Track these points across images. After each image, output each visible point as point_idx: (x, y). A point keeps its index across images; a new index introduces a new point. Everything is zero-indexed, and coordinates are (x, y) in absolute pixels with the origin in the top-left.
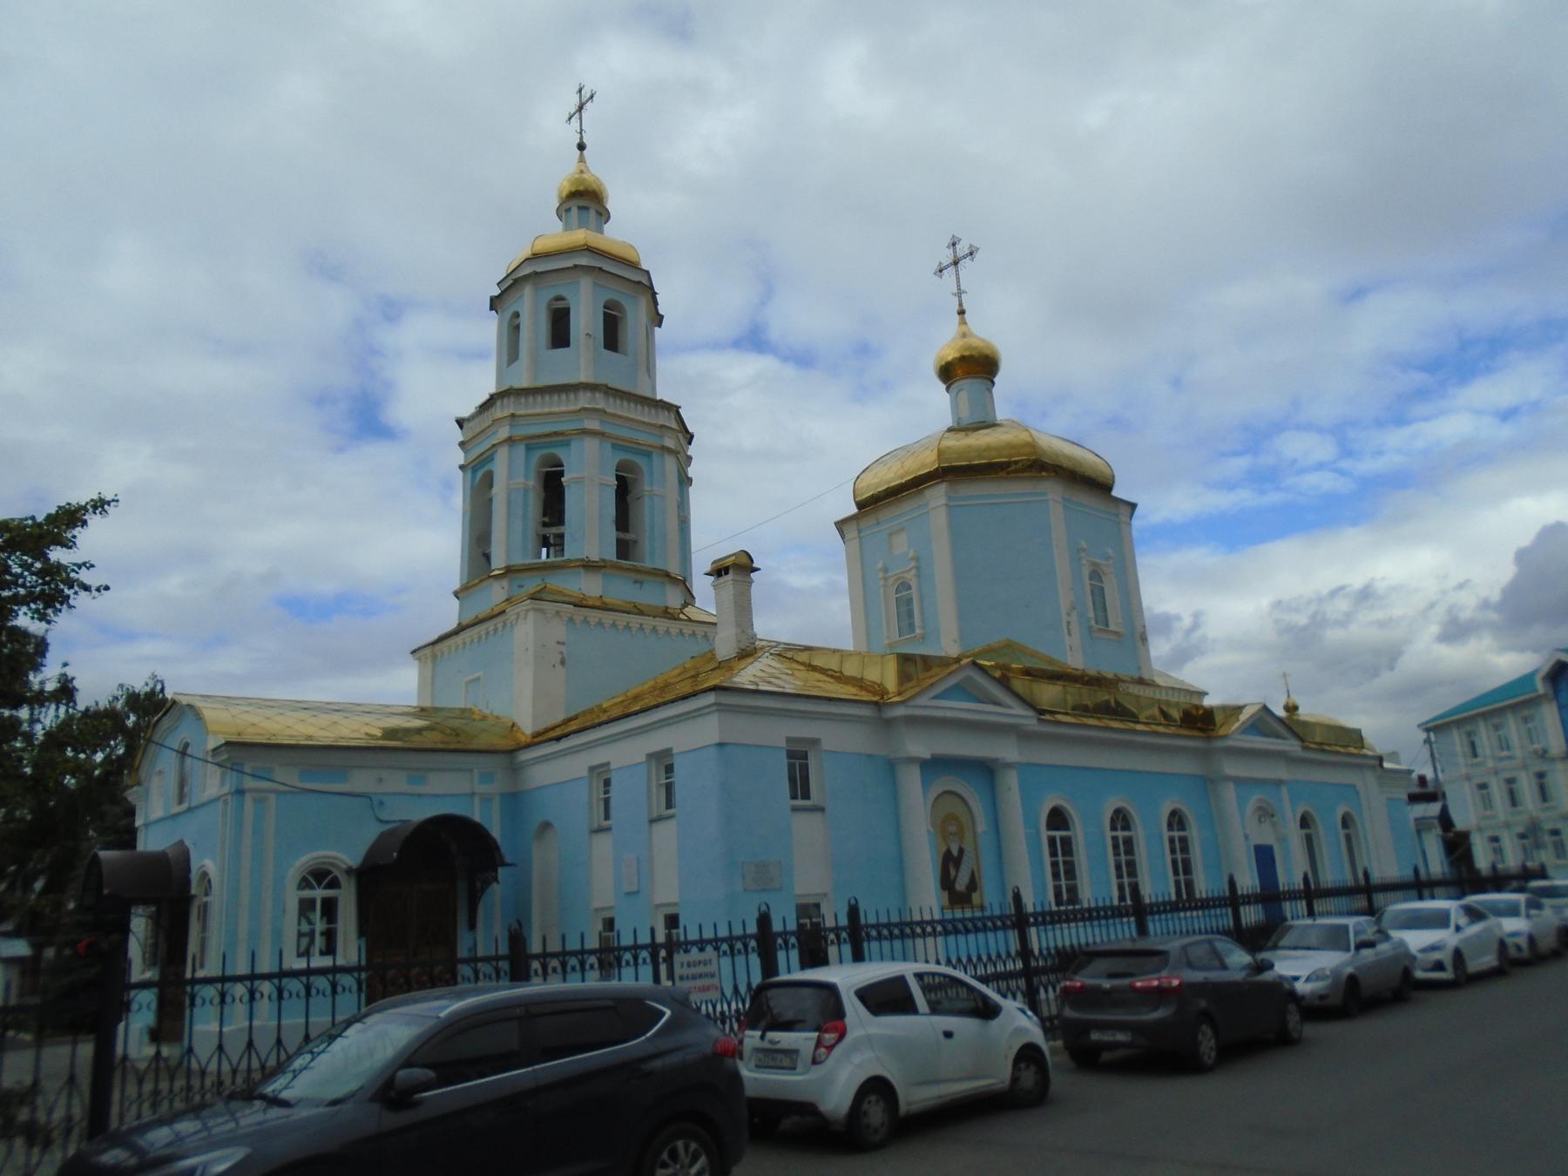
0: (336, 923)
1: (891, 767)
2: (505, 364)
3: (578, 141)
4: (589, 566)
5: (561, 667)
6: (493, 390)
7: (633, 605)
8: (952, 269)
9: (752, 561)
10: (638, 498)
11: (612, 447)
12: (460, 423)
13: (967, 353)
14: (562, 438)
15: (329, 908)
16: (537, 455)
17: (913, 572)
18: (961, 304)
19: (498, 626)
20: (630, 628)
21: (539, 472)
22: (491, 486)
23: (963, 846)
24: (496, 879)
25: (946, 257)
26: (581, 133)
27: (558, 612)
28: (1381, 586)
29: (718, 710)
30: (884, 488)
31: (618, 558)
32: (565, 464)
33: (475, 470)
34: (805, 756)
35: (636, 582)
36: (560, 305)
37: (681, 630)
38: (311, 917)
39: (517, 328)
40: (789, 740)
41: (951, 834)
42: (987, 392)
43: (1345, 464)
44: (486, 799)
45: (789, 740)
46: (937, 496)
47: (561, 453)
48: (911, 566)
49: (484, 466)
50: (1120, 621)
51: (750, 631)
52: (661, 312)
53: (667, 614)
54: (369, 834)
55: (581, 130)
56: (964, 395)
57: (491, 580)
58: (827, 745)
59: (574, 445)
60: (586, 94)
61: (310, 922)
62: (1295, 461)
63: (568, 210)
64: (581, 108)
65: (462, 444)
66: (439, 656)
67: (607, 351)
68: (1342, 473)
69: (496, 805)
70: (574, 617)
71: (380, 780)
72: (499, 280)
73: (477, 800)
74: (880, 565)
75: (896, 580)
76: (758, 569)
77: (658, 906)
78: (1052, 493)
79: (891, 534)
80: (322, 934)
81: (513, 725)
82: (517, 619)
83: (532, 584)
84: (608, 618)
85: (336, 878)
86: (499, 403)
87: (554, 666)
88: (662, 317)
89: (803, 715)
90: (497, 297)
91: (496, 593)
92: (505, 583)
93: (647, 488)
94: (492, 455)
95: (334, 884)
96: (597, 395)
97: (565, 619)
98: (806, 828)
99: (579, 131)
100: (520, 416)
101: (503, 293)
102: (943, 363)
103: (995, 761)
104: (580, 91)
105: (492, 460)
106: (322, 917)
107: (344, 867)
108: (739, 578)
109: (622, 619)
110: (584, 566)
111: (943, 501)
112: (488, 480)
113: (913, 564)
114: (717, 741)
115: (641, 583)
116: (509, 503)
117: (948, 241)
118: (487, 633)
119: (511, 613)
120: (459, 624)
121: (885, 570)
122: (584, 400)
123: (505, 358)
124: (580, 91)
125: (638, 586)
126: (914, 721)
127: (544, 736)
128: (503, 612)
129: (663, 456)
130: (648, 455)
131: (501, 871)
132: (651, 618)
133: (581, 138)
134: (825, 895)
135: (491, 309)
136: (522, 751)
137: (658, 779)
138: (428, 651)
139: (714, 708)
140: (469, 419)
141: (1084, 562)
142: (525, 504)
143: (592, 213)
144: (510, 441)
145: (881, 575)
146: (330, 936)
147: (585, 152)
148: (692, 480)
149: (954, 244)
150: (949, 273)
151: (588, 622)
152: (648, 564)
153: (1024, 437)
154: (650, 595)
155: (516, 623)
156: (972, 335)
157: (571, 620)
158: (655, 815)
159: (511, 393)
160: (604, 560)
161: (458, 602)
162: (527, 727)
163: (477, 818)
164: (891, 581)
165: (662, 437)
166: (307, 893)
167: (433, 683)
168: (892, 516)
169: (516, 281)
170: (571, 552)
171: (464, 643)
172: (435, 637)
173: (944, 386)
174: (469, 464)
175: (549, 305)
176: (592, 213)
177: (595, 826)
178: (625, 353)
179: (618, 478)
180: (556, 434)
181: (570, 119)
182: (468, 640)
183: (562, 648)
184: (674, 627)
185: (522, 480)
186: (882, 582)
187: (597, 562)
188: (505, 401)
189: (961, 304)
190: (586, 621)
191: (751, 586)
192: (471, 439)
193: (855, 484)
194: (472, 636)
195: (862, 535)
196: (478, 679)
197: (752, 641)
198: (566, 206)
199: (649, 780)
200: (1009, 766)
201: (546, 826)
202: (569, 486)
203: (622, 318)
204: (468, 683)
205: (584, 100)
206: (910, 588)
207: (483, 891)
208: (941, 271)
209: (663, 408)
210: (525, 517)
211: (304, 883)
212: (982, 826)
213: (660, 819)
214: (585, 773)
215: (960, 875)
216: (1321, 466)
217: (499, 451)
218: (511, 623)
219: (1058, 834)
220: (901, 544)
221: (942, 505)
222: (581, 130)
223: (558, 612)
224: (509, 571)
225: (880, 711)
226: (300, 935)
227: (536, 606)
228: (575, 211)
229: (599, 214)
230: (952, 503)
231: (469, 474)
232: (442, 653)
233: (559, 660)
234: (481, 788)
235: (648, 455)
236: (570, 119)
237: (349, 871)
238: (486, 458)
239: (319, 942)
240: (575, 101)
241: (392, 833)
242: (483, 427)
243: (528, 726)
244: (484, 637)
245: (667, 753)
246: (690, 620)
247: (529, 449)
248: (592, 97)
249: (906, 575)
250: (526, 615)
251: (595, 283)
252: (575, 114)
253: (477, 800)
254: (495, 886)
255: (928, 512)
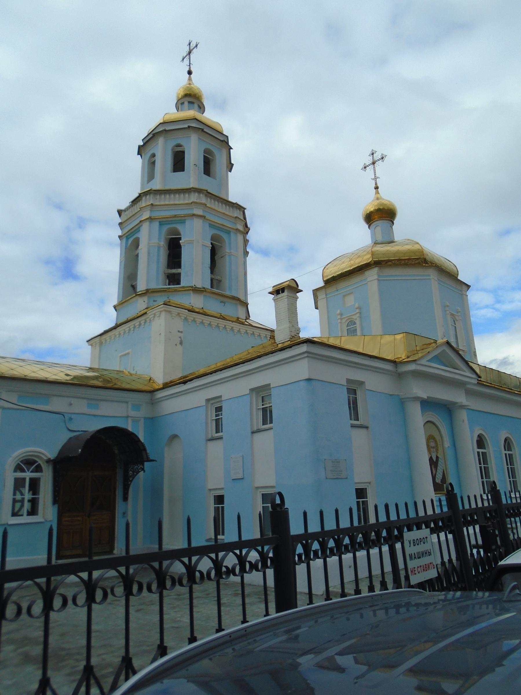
0: (39, 495)
1: (402, 402)
2: (146, 182)
3: (188, 69)
4: (196, 290)
5: (180, 345)
6: (140, 192)
7: (220, 314)
8: (372, 166)
9: (298, 286)
10: (222, 257)
11: (209, 226)
12: (120, 212)
13: (381, 207)
14: (182, 219)
15: (34, 485)
16: (166, 228)
17: (358, 315)
18: (376, 184)
19: (142, 322)
20: (219, 327)
21: (166, 238)
22: (137, 246)
23: (438, 455)
24: (143, 469)
25: (368, 160)
26: (190, 65)
27: (179, 314)
28: (511, 359)
29: (307, 357)
30: (340, 272)
31: (211, 288)
32: (182, 233)
33: (128, 238)
34: (354, 392)
35: (221, 302)
36: (179, 149)
37: (246, 331)
38: (23, 491)
39: (154, 163)
40: (349, 381)
41: (432, 447)
42: (390, 228)
43: (498, 306)
44: (136, 421)
45: (349, 381)
46: (372, 274)
47: (179, 227)
48: (357, 312)
49: (134, 235)
50: (465, 345)
51: (296, 326)
52: (232, 162)
53: (238, 321)
54: (64, 437)
55: (190, 64)
56: (379, 229)
57: (137, 297)
58: (368, 386)
59: (188, 222)
60: (193, 45)
61: (22, 494)
62: (476, 304)
63: (183, 103)
64: (190, 53)
65: (120, 224)
66: (104, 342)
67: (205, 175)
68: (497, 310)
69: (142, 423)
70: (188, 317)
71: (71, 404)
72: (143, 138)
73: (130, 420)
74: (338, 312)
75: (347, 320)
76: (301, 291)
77: (257, 488)
78: (432, 275)
79: (344, 296)
80: (29, 501)
81: (150, 379)
82: (154, 317)
83: (161, 299)
84: (207, 320)
85: (39, 465)
86: (144, 198)
87: (176, 345)
88: (232, 165)
89: (357, 366)
90: (142, 146)
91: (140, 304)
92: (145, 298)
93: (227, 251)
94: (139, 228)
95: (39, 469)
96: (201, 195)
97: (183, 318)
98: (358, 436)
99: (188, 65)
100: (156, 205)
101: (144, 144)
102: (368, 212)
103: (454, 403)
104: (190, 44)
105: (139, 231)
106: (29, 490)
107: (45, 458)
108: (290, 295)
109: (215, 321)
110: (192, 290)
111: (376, 277)
112: (136, 244)
113: (358, 311)
114: (307, 377)
115: (224, 303)
116: (149, 253)
117: (370, 152)
118: (134, 327)
119: (149, 314)
120: (116, 324)
121: (341, 314)
122: (194, 197)
123: (146, 179)
124: (190, 44)
125: (223, 304)
126: (418, 375)
127: (166, 386)
128: (146, 313)
129: (236, 234)
130: (228, 233)
131: (146, 464)
132: (231, 322)
133: (190, 68)
134: (370, 483)
135: (138, 154)
136: (159, 392)
137: (257, 405)
138: (97, 339)
139: (306, 355)
140: (125, 211)
141: (448, 312)
142: (158, 256)
143: (196, 106)
144: (151, 219)
145: (339, 317)
146: (34, 502)
147: (191, 75)
148: (249, 253)
149: (373, 154)
150: (370, 169)
151: (195, 321)
152: (228, 293)
153: (416, 247)
154: (229, 310)
155: (153, 319)
156: (381, 198)
157: (186, 319)
158: (255, 429)
159: (151, 193)
160: (204, 288)
161: (116, 312)
162: (160, 381)
163: (130, 429)
164: (344, 321)
165: (235, 224)
166: (221, 417)
167: (100, 358)
168: (344, 286)
169: (154, 135)
170: (184, 282)
171: (120, 334)
172: (101, 331)
173: (367, 226)
174: (125, 234)
175: (173, 149)
176: (196, 106)
177: (210, 437)
178: (215, 178)
179: (212, 244)
180: (175, 216)
181: (183, 60)
182: (122, 332)
183: (180, 334)
184: (243, 329)
185: (157, 241)
186: (339, 321)
187: (201, 288)
188: (148, 197)
189: (376, 184)
190: (194, 320)
191: (297, 300)
192: (124, 222)
193: (323, 271)
194: (124, 330)
195: (327, 297)
196: (128, 354)
197: (297, 332)
198: (180, 102)
199: (251, 404)
200: (462, 407)
201: (175, 437)
202: (184, 245)
203: (213, 160)
204: (121, 356)
205: (191, 48)
206: (355, 323)
207: (134, 477)
208: (365, 168)
209: (237, 208)
210: (158, 262)
211: (18, 468)
212: (447, 444)
213: (259, 431)
214: (248, 392)
215: (437, 473)
216: (487, 307)
217: (143, 224)
218: (150, 320)
219: (481, 450)
220: (351, 301)
221: (376, 279)
222: (190, 64)
223: (179, 314)
224: (147, 292)
225: (396, 368)
226: (15, 501)
227: (166, 309)
228: (186, 103)
229: (200, 107)
230: (380, 279)
231: (124, 240)
232: (106, 340)
233: (179, 342)
234: (132, 413)
235: (228, 233)
236: (183, 60)
237: (48, 461)
238: (136, 229)
239: (27, 506)
240: (187, 49)
241: (76, 438)
242: (134, 213)
243: (160, 380)
244: (132, 329)
245: (267, 387)
246: (250, 325)
247: (161, 224)
248: (196, 46)
249: (353, 317)
250: (160, 314)
251: (199, 138)
252: (186, 56)
253: (130, 420)
254: (141, 473)
255: (367, 283)
